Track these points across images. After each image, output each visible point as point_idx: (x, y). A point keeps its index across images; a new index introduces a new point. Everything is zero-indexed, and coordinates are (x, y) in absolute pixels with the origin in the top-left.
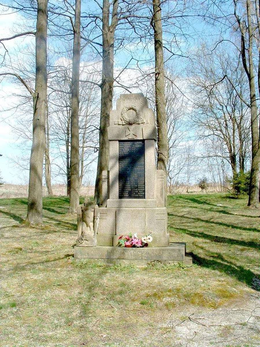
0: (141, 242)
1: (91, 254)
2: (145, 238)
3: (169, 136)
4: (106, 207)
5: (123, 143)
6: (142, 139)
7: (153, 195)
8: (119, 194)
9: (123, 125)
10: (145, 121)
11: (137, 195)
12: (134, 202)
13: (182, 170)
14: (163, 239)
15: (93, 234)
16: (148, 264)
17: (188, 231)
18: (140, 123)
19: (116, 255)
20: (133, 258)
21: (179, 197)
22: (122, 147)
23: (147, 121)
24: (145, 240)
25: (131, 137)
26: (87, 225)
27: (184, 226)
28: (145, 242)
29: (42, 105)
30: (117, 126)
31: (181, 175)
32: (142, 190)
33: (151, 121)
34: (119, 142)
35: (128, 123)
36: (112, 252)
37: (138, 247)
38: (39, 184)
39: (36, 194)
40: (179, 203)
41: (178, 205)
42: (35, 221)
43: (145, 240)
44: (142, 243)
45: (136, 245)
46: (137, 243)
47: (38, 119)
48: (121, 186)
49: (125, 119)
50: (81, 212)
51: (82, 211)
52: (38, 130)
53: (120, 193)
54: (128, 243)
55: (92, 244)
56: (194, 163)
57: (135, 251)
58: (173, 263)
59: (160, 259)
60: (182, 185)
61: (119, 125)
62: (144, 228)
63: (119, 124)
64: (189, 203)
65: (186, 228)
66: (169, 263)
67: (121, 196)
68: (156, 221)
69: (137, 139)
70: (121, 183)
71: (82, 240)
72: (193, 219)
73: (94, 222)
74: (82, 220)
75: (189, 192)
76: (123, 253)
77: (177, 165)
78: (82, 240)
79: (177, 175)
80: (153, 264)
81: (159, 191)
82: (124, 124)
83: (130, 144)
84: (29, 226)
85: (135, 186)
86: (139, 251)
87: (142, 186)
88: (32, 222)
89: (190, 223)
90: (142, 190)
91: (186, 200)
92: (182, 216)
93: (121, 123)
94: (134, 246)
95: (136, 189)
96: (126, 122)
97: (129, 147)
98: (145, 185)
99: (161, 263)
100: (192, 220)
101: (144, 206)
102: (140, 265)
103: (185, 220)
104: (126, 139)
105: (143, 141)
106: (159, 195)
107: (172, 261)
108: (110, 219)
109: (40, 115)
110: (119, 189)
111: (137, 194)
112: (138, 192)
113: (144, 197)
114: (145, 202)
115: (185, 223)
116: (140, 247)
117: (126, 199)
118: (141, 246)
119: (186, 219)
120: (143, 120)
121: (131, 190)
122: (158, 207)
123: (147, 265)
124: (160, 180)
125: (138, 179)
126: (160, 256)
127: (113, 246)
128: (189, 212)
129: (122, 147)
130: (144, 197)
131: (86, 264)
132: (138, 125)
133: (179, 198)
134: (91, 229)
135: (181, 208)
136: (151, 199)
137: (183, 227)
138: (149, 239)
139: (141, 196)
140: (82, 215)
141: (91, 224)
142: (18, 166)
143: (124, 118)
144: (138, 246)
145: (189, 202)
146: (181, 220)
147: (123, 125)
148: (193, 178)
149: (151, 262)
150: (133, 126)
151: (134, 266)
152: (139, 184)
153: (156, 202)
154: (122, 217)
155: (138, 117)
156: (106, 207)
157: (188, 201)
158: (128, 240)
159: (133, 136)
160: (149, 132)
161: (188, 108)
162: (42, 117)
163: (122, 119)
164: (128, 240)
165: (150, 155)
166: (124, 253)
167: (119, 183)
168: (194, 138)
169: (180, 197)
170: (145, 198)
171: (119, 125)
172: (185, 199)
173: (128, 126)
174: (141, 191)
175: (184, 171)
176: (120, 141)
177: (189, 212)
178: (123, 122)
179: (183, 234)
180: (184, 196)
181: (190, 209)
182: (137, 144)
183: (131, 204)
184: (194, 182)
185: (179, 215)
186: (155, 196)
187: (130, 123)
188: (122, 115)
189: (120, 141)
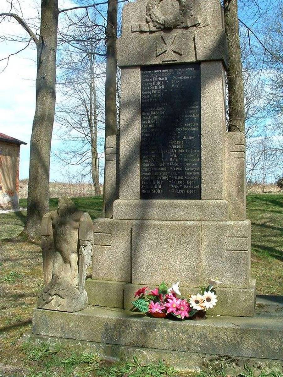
0: (187, 307)
1: (69, 328)
2: (199, 297)
3: (246, 111)
4: (112, 218)
5: (152, 73)
6: (194, 60)
7: (220, 191)
8: (141, 189)
9: (151, 32)
10: (200, 21)
11: (181, 191)
12: (175, 206)
13: (256, 166)
14: (242, 297)
15: (76, 282)
16: (203, 364)
17: (276, 253)
18: (189, 25)
19: (130, 336)
20: (167, 345)
21: (255, 197)
22: (150, 82)
23: (205, 20)
24: (197, 302)
25: (170, 57)
26: (66, 260)
27: (268, 241)
28: (197, 307)
29: (49, 56)
30: (138, 35)
31: (256, 171)
32: (194, 178)
33: (214, 21)
34: (142, 70)
35: (162, 27)
36: (120, 327)
37: (180, 320)
38: (44, 177)
39: (39, 191)
40: (256, 206)
41: (254, 208)
42: (36, 232)
43: (197, 302)
44: (190, 310)
45: (176, 314)
46: (178, 310)
47: (43, 78)
48: (146, 170)
49: (154, 19)
50: (51, 228)
51: (54, 226)
52: (43, 93)
53: (145, 185)
54: (157, 308)
55: (70, 306)
56: (271, 157)
57: (172, 329)
58: (270, 367)
59: (234, 355)
60: (256, 184)
61: (142, 32)
62: (196, 269)
63: (143, 29)
64: (269, 206)
65: (272, 245)
66: (259, 368)
67: (147, 193)
68: (226, 253)
69: (183, 61)
70: (145, 163)
71: (50, 294)
72: (278, 229)
73: (78, 252)
74: (53, 247)
75: (266, 192)
76: (144, 333)
77: (251, 160)
78: (50, 294)
79: (251, 172)
80: (217, 365)
81: (234, 183)
82: (153, 29)
83: (167, 73)
84: (28, 240)
85: (177, 169)
86: (182, 331)
87: (194, 169)
88: (32, 235)
89: (276, 237)
90: (194, 178)
91: (265, 202)
92: (263, 225)
93: (145, 28)
94: (171, 317)
95: (180, 178)
96: (158, 26)
97: (164, 81)
98: (201, 167)
99: (237, 365)
100: (278, 231)
101: (199, 217)
102: (183, 365)
103: (267, 232)
104: (157, 63)
105: (197, 64)
106: (234, 190)
107: (267, 362)
108: (119, 246)
109: (47, 72)
110: (141, 176)
111: (182, 188)
112: (186, 184)
113: (197, 195)
114: (202, 206)
115: (269, 236)
116: (186, 318)
117: (159, 201)
118: (188, 316)
119: (269, 230)
120: (196, 19)
121: (170, 179)
122: (231, 219)
123: (201, 368)
124: (236, 156)
125: (185, 152)
126: (236, 346)
127: (123, 308)
128: (271, 218)
129: (150, 82)
130: (197, 195)
131: (55, 353)
132: (183, 30)
133: (255, 199)
134: (73, 268)
135: (260, 212)
136: (214, 201)
137: (266, 244)
138: (208, 300)
139: (191, 192)
140: (55, 234)
141: (74, 257)
142: (59, 160)
143: (153, 15)
144: (179, 317)
145: (269, 205)
146: (261, 231)
147: (151, 32)
148: (270, 175)
149: (211, 361)
150: (177, 33)
151: (167, 366)
152: (187, 164)
153: (226, 207)
154: (148, 243)
155: (184, 14)
156: (112, 218)
157: (268, 203)
158: (157, 298)
159: (174, 54)
160: (211, 44)
161: (265, 89)
162: (49, 74)
163: (149, 19)
164: (157, 298)
165: (214, 96)
166: (145, 334)
167: (141, 163)
168: (271, 127)
169: (257, 198)
170: (200, 199)
171: (142, 32)
172: (264, 200)
173: (162, 33)
174: (192, 180)
175: (260, 166)
176: (144, 68)
177: (272, 219)
178: (151, 24)
179: (270, 259)
180: (261, 197)
181: (272, 214)
182: (183, 73)
183: (171, 212)
184: (271, 180)
185: (258, 223)
186: (225, 194)
187: (167, 25)
188: (148, 10)
189: (144, 68)
